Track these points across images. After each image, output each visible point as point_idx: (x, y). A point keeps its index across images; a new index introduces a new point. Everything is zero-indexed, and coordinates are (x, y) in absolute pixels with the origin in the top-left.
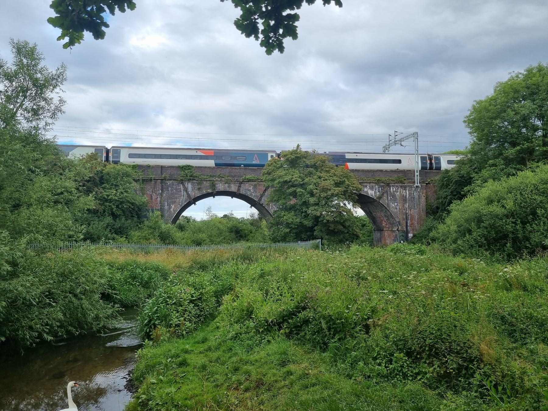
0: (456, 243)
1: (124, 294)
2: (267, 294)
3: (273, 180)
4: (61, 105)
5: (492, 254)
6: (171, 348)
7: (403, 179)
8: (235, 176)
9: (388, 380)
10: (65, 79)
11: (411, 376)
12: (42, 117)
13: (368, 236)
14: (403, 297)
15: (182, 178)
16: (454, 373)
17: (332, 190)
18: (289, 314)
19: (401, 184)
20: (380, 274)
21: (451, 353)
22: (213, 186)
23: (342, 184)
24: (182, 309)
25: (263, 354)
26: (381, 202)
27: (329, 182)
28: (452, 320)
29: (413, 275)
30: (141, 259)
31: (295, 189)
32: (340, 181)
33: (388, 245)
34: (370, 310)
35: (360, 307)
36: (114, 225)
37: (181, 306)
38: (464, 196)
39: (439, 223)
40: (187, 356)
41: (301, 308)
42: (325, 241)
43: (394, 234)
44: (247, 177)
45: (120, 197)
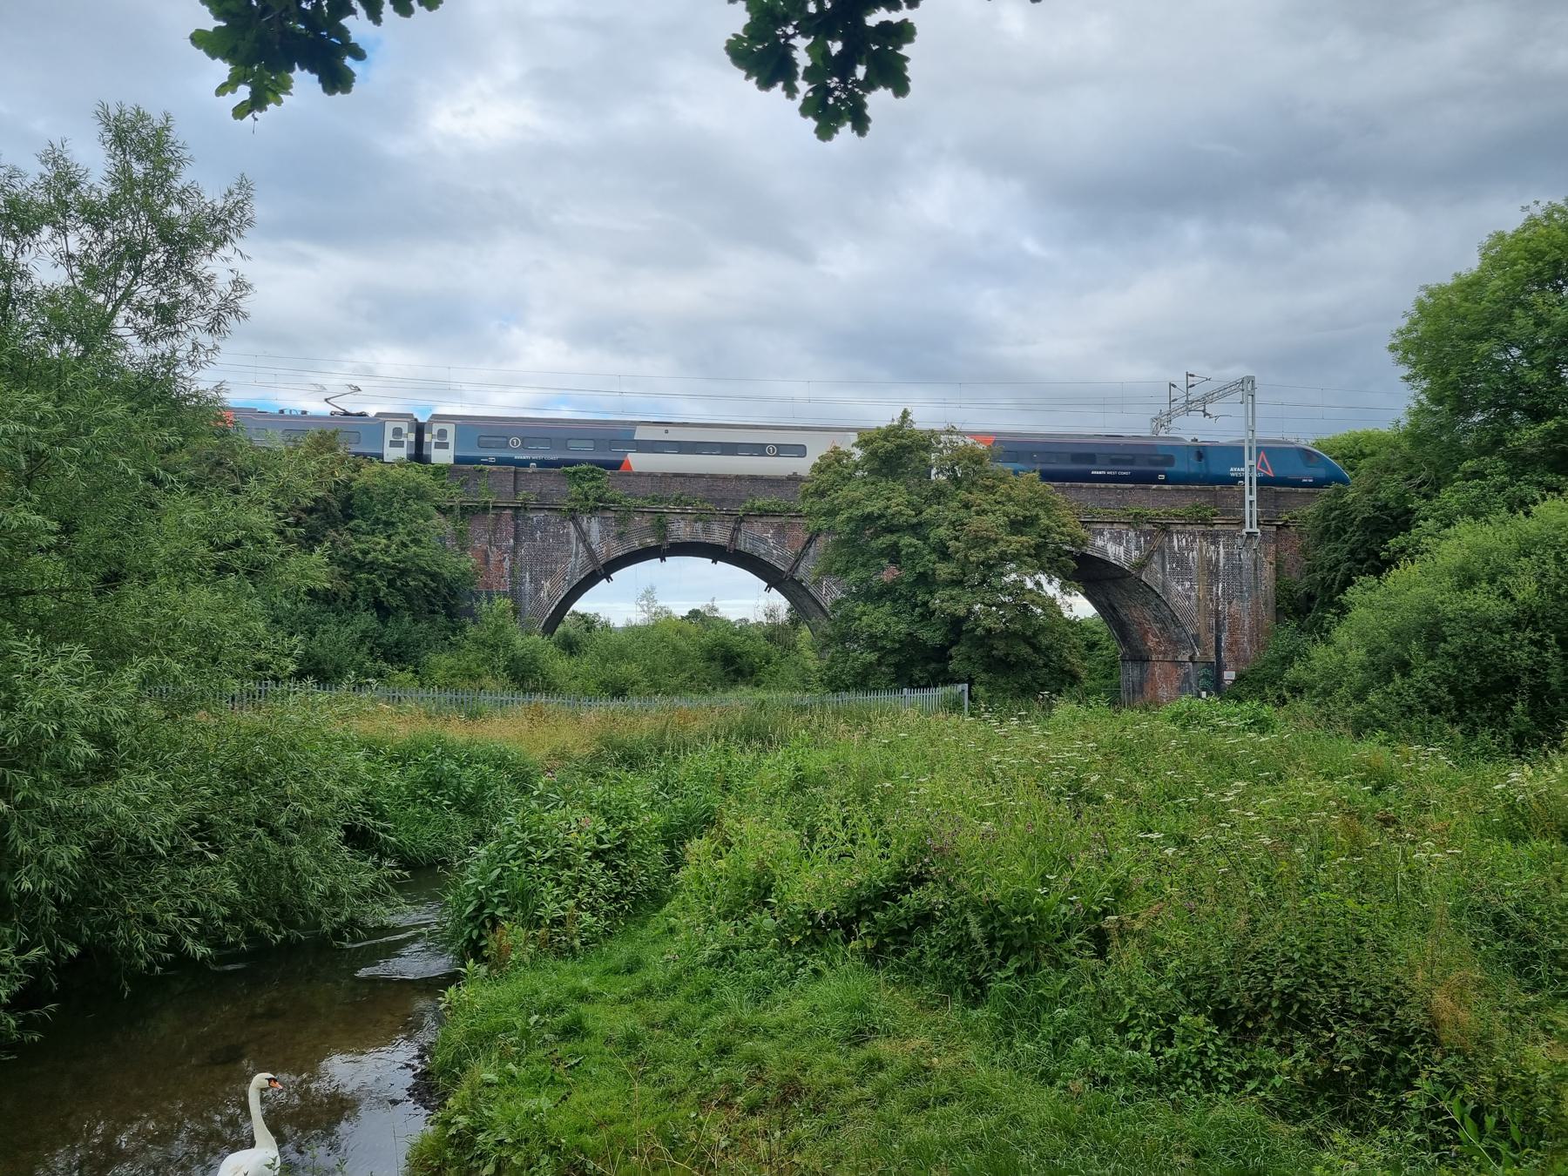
1: (407, 830)
2: (812, 839)
3: (832, 513)
4: (238, 294)
5: (1471, 734)
6: (539, 984)
7: (1208, 513)
8: (723, 500)
10: (250, 222)
11: (1229, 1081)
12: (185, 328)
13: (1106, 677)
14: (1205, 852)
15: (572, 504)
16: (1353, 1074)
17: (1000, 543)
19: (1202, 528)
20: (1140, 786)
21: (1347, 1017)
22: (661, 527)
24: (570, 877)
26: (1143, 578)
29: (1235, 791)
30: (457, 732)
31: (894, 538)
32: (1025, 517)
33: (1162, 703)
34: (1108, 889)
35: (1080, 880)
36: (381, 636)
37: (569, 867)
38: (1390, 563)
39: (1314, 640)
40: (583, 1008)
41: (911, 880)
42: (980, 690)
43: (1181, 672)
44: (758, 504)
45: (400, 557)
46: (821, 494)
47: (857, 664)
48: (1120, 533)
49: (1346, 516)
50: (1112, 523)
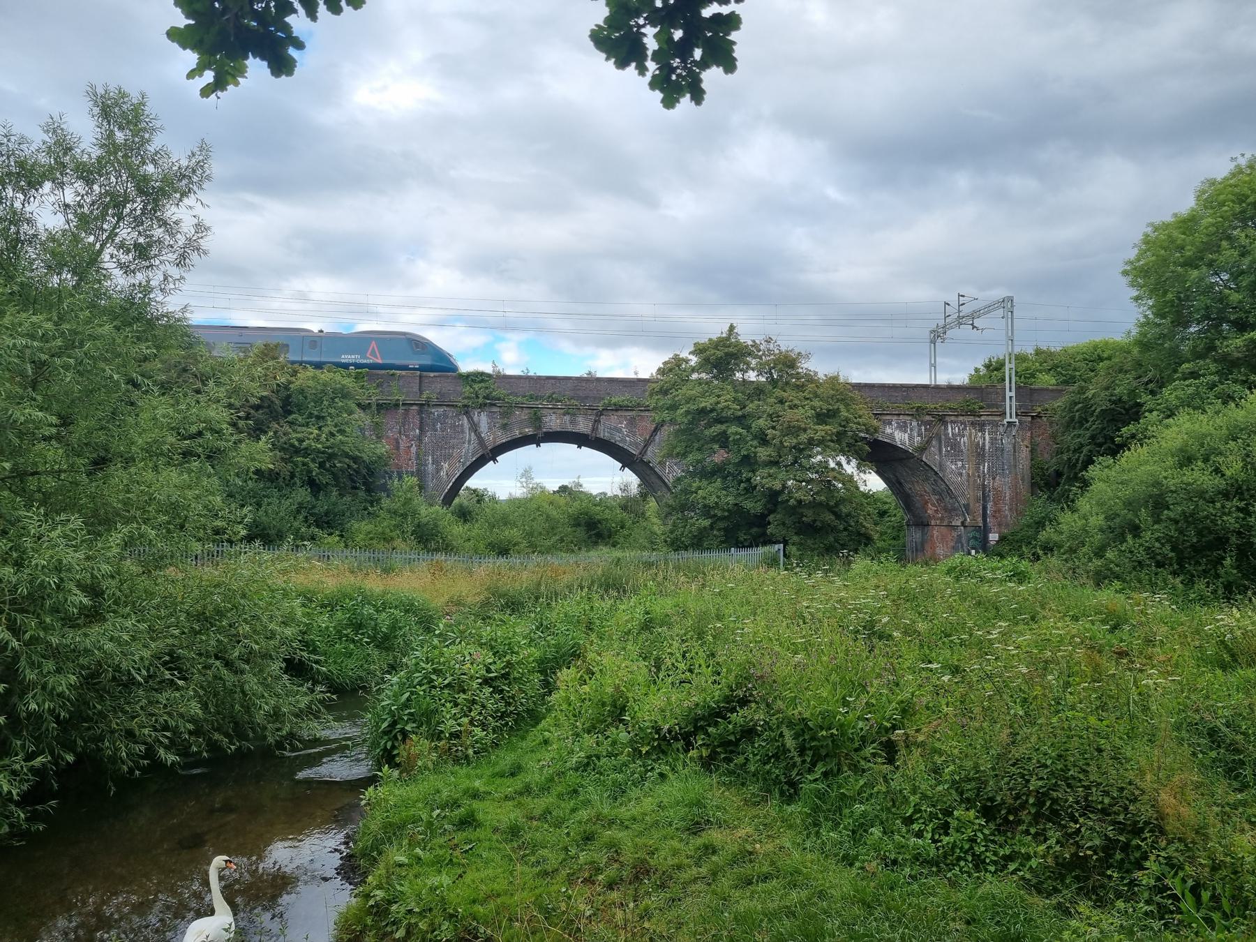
0: (1102, 557)
1: (335, 662)
2: (658, 668)
3: (673, 407)
4: (200, 235)
5: (1189, 583)
6: (440, 785)
7: (976, 407)
8: (586, 398)
9: (939, 871)
10: (209, 178)
11: (995, 863)
12: (157, 262)
13: (894, 539)
15: (466, 402)
16: (1095, 857)
17: (809, 431)
18: (710, 715)
19: (971, 418)
20: (922, 626)
22: (537, 420)
23: (834, 416)
24: (465, 699)
25: (648, 803)
27: (802, 411)
28: (1091, 736)
29: (998, 630)
30: (374, 584)
31: (723, 427)
32: (829, 410)
34: (896, 709)
35: (873, 701)
36: (314, 507)
37: (464, 691)
38: (1123, 446)
40: (476, 804)
41: (738, 702)
42: (793, 549)
43: (955, 534)
44: (614, 400)
45: (328, 444)
46: (664, 392)
47: (694, 529)
48: (905, 422)
49: (1087, 409)
50: (899, 415)
